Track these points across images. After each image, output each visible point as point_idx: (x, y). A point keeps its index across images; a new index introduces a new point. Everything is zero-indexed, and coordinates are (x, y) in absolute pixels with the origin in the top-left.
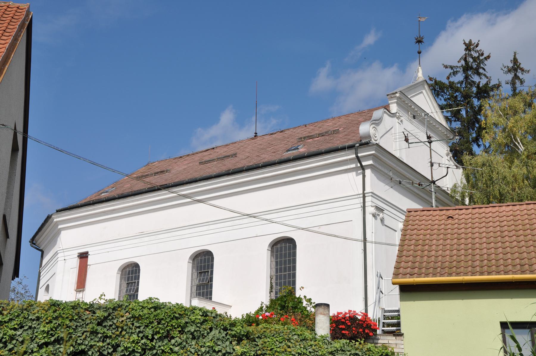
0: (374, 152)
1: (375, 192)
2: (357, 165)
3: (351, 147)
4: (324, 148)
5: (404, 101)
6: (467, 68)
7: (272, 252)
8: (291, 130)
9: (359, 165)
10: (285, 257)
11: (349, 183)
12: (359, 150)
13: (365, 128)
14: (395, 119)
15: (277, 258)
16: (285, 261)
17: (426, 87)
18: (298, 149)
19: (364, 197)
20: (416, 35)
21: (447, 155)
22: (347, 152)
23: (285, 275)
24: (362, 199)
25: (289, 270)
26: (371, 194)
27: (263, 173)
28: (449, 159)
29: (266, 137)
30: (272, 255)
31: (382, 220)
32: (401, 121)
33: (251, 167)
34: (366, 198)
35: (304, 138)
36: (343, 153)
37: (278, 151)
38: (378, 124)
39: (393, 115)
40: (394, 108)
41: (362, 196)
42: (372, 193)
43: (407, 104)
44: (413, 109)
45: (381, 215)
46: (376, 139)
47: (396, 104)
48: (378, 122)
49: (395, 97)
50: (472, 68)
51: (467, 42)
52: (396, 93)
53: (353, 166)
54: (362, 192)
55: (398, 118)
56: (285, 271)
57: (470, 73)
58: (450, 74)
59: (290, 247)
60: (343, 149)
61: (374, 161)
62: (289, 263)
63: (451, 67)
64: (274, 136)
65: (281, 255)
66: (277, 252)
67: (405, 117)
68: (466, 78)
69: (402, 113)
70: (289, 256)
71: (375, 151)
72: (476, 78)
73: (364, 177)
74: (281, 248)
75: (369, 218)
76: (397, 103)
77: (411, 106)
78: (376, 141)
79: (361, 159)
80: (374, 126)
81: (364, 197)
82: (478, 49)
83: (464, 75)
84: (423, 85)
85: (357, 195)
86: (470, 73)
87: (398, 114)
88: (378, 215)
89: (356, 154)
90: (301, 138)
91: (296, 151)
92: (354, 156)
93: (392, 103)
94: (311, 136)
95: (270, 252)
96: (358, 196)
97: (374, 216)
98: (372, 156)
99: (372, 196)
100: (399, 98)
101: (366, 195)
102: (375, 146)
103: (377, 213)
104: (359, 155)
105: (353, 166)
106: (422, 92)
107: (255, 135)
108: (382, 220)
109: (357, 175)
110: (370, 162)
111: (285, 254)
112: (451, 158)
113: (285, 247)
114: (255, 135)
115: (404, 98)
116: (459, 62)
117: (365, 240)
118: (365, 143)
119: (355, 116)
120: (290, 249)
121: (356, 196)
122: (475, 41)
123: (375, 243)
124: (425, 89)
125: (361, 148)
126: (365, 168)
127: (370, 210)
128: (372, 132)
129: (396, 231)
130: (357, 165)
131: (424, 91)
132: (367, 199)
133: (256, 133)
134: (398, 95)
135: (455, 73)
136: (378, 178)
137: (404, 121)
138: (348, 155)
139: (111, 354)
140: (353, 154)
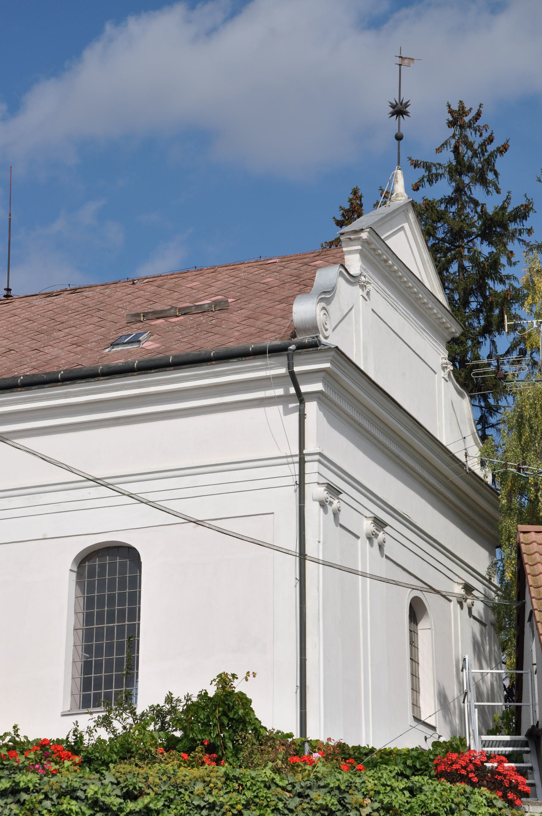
0: (327, 365)
1: (325, 453)
2: (287, 390)
3: (276, 351)
4: (209, 344)
5: (374, 250)
6: (459, 169)
7: (80, 574)
8: (98, 289)
9: (292, 390)
10: (112, 587)
11: (268, 429)
12: (296, 358)
13: (304, 309)
14: (357, 290)
15: (91, 588)
16: (111, 598)
17: (412, 216)
18: (139, 341)
19: (302, 463)
20: (394, 98)
21: (444, 368)
22: (269, 361)
23: (110, 630)
24: (297, 466)
25: (121, 617)
26: (317, 457)
27: (66, 395)
28: (446, 377)
29: (37, 301)
30: (79, 582)
31: (336, 514)
32: (368, 293)
33: (35, 379)
34: (308, 466)
35: (145, 315)
36: (258, 363)
37: (86, 341)
38: (328, 301)
39: (353, 280)
40: (354, 263)
41: (297, 459)
42: (320, 454)
43: (379, 255)
44: (390, 266)
45: (335, 502)
46: (326, 334)
47: (357, 256)
48: (327, 296)
49: (360, 238)
50: (470, 168)
51: (455, 107)
52: (362, 230)
53: (280, 392)
54: (297, 452)
55: (363, 287)
56: (111, 619)
57: (466, 180)
58: (422, 180)
59: (123, 565)
60: (259, 353)
61: (325, 385)
62: (122, 602)
63: (428, 167)
64: (58, 300)
65: (102, 583)
66: (91, 574)
67: (375, 285)
68: (459, 190)
69: (369, 276)
70: (122, 585)
71: (332, 362)
72: (478, 192)
73: (302, 418)
74: (102, 567)
75: (312, 508)
76: (361, 252)
77: (386, 261)
78: (326, 338)
79: (299, 379)
80: (323, 304)
81: (302, 463)
82: (480, 123)
83: (454, 184)
84: (406, 212)
85: (287, 457)
86: (466, 180)
87: (363, 278)
88: (331, 503)
89: (290, 367)
90: (138, 315)
91: (135, 346)
92: (283, 371)
93: (350, 252)
94: (162, 311)
95: (74, 575)
96: (290, 460)
97: (323, 504)
98: (323, 374)
99: (319, 461)
100: (366, 242)
101: (307, 458)
102: (332, 353)
103: (330, 499)
104: (296, 369)
105: (280, 392)
106: (402, 228)
107: (5, 293)
108: (336, 514)
109: (287, 412)
110: (318, 387)
111: (112, 582)
112: (449, 375)
113: (112, 566)
114: (5, 293)
115: (376, 244)
116: (438, 150)
117: (302, 556)
118: (305, 343)
119: (251, 270)
120: (123, 571)
121: (284, 460)
122: (471, 105)
123: (326, 564)
124: (408, 220)
125: (300, 354)
126: (305, 397)
127: (315, 491)
128: (320, 317)
129: (358, 537)
130: (287, 390)
131: (406, 225)
132: (309, 467)
133: (8, 290)
134: (364, 235)
135: (432, 179)
136: (329, 422)
137: (373, 293)
138: (271, 368)
139: (158, 812)
140: (281, 366)
